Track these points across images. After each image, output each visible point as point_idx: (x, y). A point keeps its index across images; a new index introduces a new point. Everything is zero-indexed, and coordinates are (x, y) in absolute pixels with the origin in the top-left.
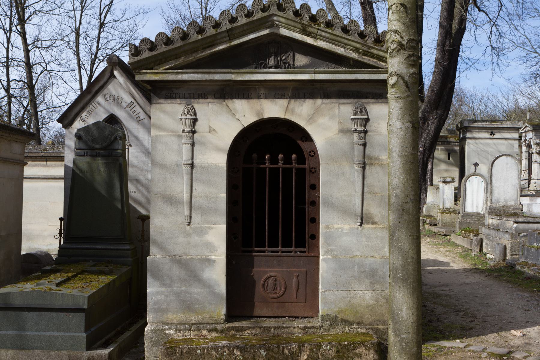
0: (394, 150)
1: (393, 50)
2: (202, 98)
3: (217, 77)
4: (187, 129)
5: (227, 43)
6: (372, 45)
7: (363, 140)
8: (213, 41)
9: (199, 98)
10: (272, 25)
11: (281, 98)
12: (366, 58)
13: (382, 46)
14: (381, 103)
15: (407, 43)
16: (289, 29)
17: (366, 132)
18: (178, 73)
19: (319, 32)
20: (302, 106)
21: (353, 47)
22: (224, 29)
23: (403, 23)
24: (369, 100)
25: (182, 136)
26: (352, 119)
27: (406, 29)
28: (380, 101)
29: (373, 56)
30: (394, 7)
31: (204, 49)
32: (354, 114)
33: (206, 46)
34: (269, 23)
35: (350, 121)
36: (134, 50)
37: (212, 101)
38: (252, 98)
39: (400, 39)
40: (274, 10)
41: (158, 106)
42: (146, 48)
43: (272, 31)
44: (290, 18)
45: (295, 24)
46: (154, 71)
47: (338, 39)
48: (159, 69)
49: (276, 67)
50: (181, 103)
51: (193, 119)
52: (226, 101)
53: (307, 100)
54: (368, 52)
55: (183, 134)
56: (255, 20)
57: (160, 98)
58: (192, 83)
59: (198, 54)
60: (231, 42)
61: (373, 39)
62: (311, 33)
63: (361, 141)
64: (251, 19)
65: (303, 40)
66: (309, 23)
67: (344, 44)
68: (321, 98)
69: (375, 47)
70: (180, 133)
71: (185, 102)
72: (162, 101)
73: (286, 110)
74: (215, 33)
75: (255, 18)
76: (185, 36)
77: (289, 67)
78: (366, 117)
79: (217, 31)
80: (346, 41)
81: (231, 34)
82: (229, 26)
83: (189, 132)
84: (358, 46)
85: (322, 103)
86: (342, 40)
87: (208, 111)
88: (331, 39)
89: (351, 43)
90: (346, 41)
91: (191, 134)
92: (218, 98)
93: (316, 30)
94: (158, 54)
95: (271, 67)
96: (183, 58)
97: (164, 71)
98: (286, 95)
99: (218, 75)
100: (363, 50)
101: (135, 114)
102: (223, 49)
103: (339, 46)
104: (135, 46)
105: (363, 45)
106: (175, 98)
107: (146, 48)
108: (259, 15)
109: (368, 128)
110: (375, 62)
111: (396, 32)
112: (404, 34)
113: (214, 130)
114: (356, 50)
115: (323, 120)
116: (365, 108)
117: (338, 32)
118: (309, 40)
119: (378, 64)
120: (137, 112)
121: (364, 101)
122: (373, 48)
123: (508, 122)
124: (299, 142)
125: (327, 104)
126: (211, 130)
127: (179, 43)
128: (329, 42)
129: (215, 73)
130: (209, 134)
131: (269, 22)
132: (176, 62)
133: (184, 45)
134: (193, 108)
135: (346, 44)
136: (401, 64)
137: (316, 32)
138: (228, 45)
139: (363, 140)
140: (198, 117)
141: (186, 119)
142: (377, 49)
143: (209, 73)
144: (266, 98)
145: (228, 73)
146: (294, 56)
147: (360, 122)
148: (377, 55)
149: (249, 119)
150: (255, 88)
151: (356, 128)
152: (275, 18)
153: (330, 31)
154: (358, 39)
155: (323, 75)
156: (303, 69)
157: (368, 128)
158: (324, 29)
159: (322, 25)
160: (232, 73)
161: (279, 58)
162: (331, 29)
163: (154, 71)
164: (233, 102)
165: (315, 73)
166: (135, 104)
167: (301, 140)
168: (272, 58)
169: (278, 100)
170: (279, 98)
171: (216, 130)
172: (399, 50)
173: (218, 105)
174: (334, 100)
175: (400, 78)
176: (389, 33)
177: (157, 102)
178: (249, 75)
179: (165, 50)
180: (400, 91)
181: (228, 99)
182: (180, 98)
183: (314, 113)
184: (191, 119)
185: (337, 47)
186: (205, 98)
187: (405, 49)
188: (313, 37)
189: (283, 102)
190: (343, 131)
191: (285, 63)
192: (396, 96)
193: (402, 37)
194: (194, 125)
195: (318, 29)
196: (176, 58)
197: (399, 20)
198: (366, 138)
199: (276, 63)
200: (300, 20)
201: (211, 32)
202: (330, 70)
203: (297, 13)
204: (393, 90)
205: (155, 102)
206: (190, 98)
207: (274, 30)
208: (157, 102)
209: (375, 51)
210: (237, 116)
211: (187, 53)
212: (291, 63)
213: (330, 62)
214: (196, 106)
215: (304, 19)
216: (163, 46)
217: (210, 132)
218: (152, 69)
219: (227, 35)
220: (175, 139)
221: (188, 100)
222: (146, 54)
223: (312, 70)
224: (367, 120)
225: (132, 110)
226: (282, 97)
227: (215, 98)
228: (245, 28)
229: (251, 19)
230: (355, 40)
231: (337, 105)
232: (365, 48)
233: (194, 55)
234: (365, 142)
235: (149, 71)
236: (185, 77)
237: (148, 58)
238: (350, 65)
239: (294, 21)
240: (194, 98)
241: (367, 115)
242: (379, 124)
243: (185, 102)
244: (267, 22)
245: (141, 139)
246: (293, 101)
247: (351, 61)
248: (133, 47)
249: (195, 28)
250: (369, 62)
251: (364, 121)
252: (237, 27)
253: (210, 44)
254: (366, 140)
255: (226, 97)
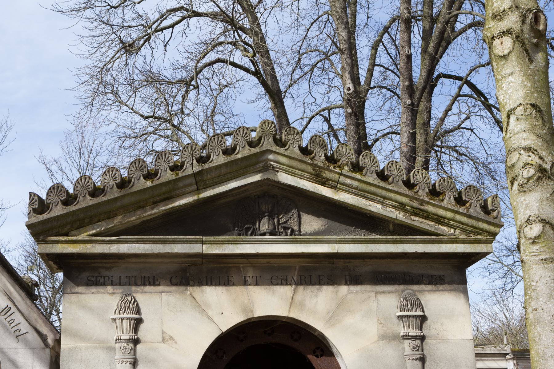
0: (548, 355)
1: (529, 179)
2: (150, 285)
3: (178, 249)
4: (125, 336)
5: (193, 195)
6: (426, 199)
7: (420, 352)
8: (170, 191)
9: (144, 285)
10: (267, 168)
11: (282, 284)
12: (417, 219)
13: (443, 200)
14: (442, 290)
15: (551, 168)
16: (293, 174)
17: (423, 338)
18: (111, 242)
19: (342, 178)
20: (316, 296)
21: (395, 201)
22: (189, 172)
23: (539, 136)
24: (423, 287)
25: (115, 349)
26: (398, 317)
27: (546, 145)
28: (441, 287)
29: (427, 216)
30: (519, 111)
31: (156, 203)
32: (402, 308)
33: (159, 198)
34: (261, 165)
35: (396, 321)
36: (37, 203)
37: (167, 288)
38: (233, 285)
39: (539, 161)
40: (268, 144)
41: (73, 297)
42: (58, 200)
43: (266, 177)
44: (296, 156)
45: (303, 166)
46: (70, 238)
47: (373, 189)
48: (79, 235)
49: (272, 234)
50: (114, 293)
51: (135, 319)
52: (191, 288)
53: (325, 288)
54: (419, 209)
55: (118, 345)
56: (239, 159)
57: (78, 285)
58: (134, 260)
59: (146, 212)
60: (199, 194)
61: (427, 190)
62: (328, 180)
63: (417, 353)
64: (233, 157)
65: (316, 191)
66: (325, 164)
67: (382, 197)
68: (346, 284)
69: (432, 201)
70: (112, 343)
71: (121, 291)
72: (80, 289)
73: (291, 303)
74: (174, 177)
75: (239, 156)
76: (123, 184)
77: (294, 234)
78: (422, 314)
79: (177, 175)
80: (384, 193)
81: (200, 180)
82: (197, 168)
83: (128, 341)
84: (404, 200)
85: (350, 292)
86: (379, 191)
87: (160, 306)
88: (361, 190)
89: (392, 195)
90: (384, 193)
91: (131, 345)
92: (176, 284)
93: (337, 176)
94: (78, 210)
95: (264, 234)
96: (119, 217)
97: (88, 238)
98: (289, 279)
99: (180, 246)
100: (412, 207)
101: (13, 325)
102: (186, 205)
103: (372, 200)
104: (40, 198)
105: (412, 198)
106: (104, 284)
107: (58, 200)
108: (244, 152)
109: (425, 332)
110: (431, 226)
111: (529, 149)
112: (544, 154)
113: (171, 338)
114: (401, 207)
115: (352, 320)
116: (418, 299)
117: (372, 179)
118: (326, 192)
119: (435, 229)
120: (17, 322)
121: (415, 287)
122: (428, 203)
123: (490, 346)
124: (311, 358)
125: (357, 292)
126: (165, 338)
127: (116, 193)
128: (356, 195)
129: (174, 242)
130: (162, 345)
131: (261, 162)
132: (108, 224)
133: (123, 196)
134: (135, 301)
135: (385, 198)
136: (545, 203)
137: (337, 179)
138: (195, 198)
139: (420, 352)
140: (143, 316)
141: (122, 319)
142: (434, 205)
143: (164, 242)
144: (257, 284)
145: (196, 242)
146: (300, 218)
147: (412, 321)
148: (434, 214)
149: (231, 319)
150: (238, 268)
151: (406, 331)
152: (271, 157)
153: (358, 176)
154: (404, 189)
155: (352, 246)
156: (317, 237)
157: (425, 332)
158: (350, 174)
159: (346, 168)
160: (203, 242)
161: (276, 221)
162: (361, 174)
163: (70, 238)
164: (202, 291)
165: (337, 242)
166: (13, 309)
167: (314, 353)
168: (265, 221)
169: (278, 287)
170: (278, 284)
171: (174, 337)
172: (539, 179)
173: (178, 296)
174: (368, 287)
175: (548, 226)
176: (516, 153)
177: (73, 290)
178: (231, 246)
179: (91, 203)
180: (549, 248)
181: (193, 285)
182: (112, 284)
183: (337, 308)
184: (131, 319)
185: (371, 203)
186: (154, 285)
187: (549, 178)
188: (331, 187)
189: (286, 291)
190: (384, 337)
191: (286, 228)
192: (541, 257)
193: (541, 158)
194: (136, 330)
195: (341, 174)
196: (109, 218)
197: (532, 130)
198: (424, 348)
199: (271, 228)
200: (312, 159)
201: (168, 176)
202: (362, 237)
203: (305, 151)
204: (536, 247)
205: (69, 290)
206: (130, 284)
207: (269, 175)
208: (73, 290)
209: (431, 209)
210: (210, 314)
211: (127, 209)
212: (296, 228)
213: (357, 227)
214: (140, 298)
215: (317, 158)
216: (88, 197)
217: (163, 341)
218: (67, 235)
219: (194, 181)
220: (102, 355)
221: (125, 287)
222: (58, 210)
223: (334, 237)
224: (424, 319)
225: (8, 319)
226: (284, 282)
227: (173, 284)
228: (224, 171)
229: (233, 157)
230: (399, 190)
231: (373, 294)
232: (415, 204)
233: (139, 212)
234: (423, 355)
235: (61, 238)
236: (124, 248)
237: (62, 216)
238: (389, 231)
239: (301, 161)
240: (136, 284)
241: (423, 311)
242: (442, 325)
243: (121, 291)
244: (257, 163)
245: (20, 364)
246: (301, 288)
247: (391, 226)
248: (36, 198)
249: (141, 169)
250: (422, 226)
251: (419, 321)
252: (210, 169)
253: (166, 196)
254: (425, 352)
255: (191, 283)
